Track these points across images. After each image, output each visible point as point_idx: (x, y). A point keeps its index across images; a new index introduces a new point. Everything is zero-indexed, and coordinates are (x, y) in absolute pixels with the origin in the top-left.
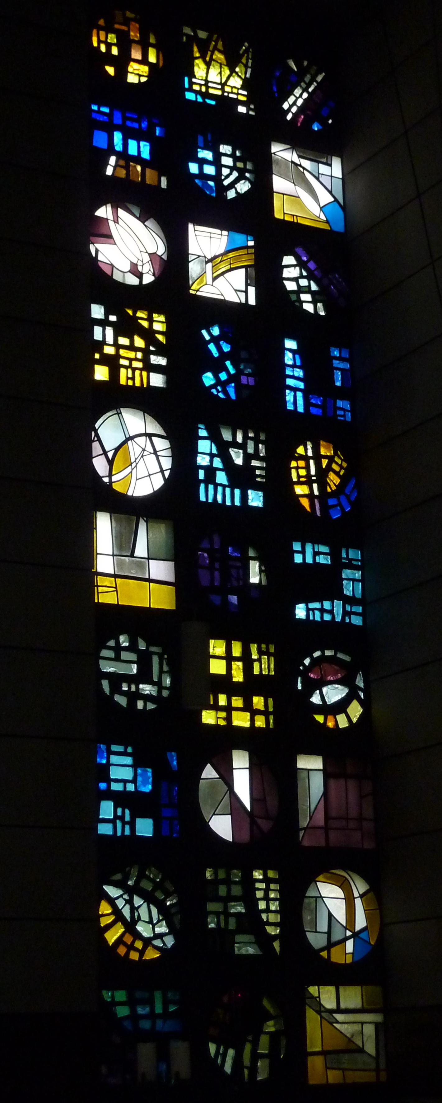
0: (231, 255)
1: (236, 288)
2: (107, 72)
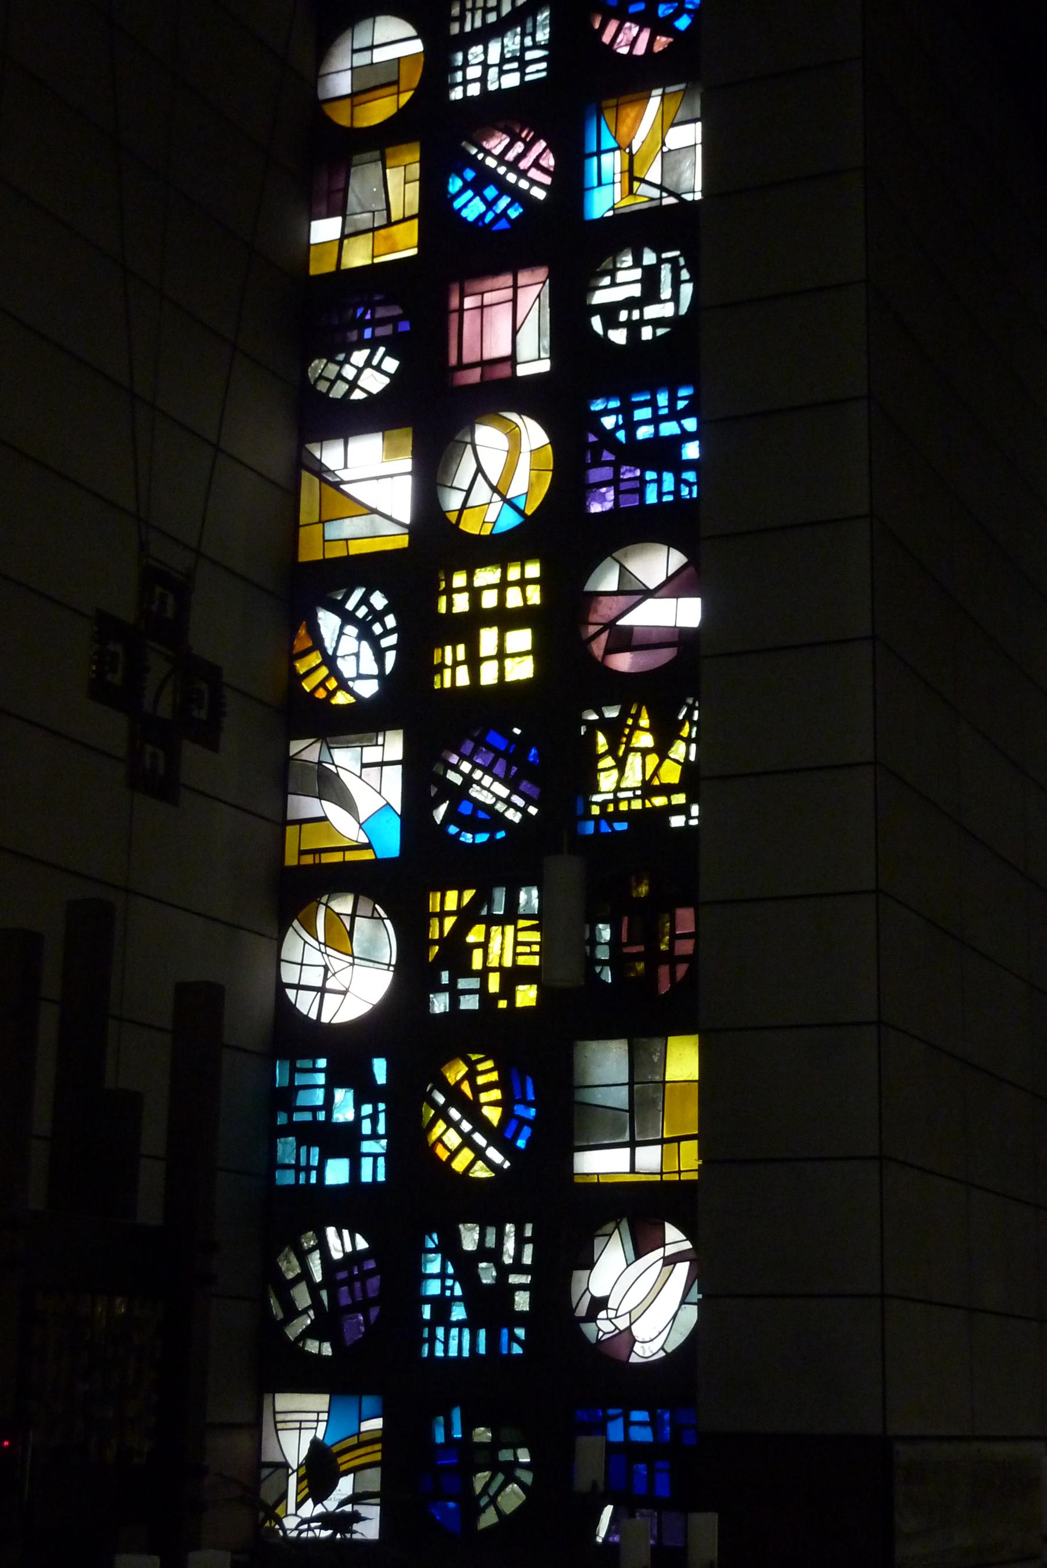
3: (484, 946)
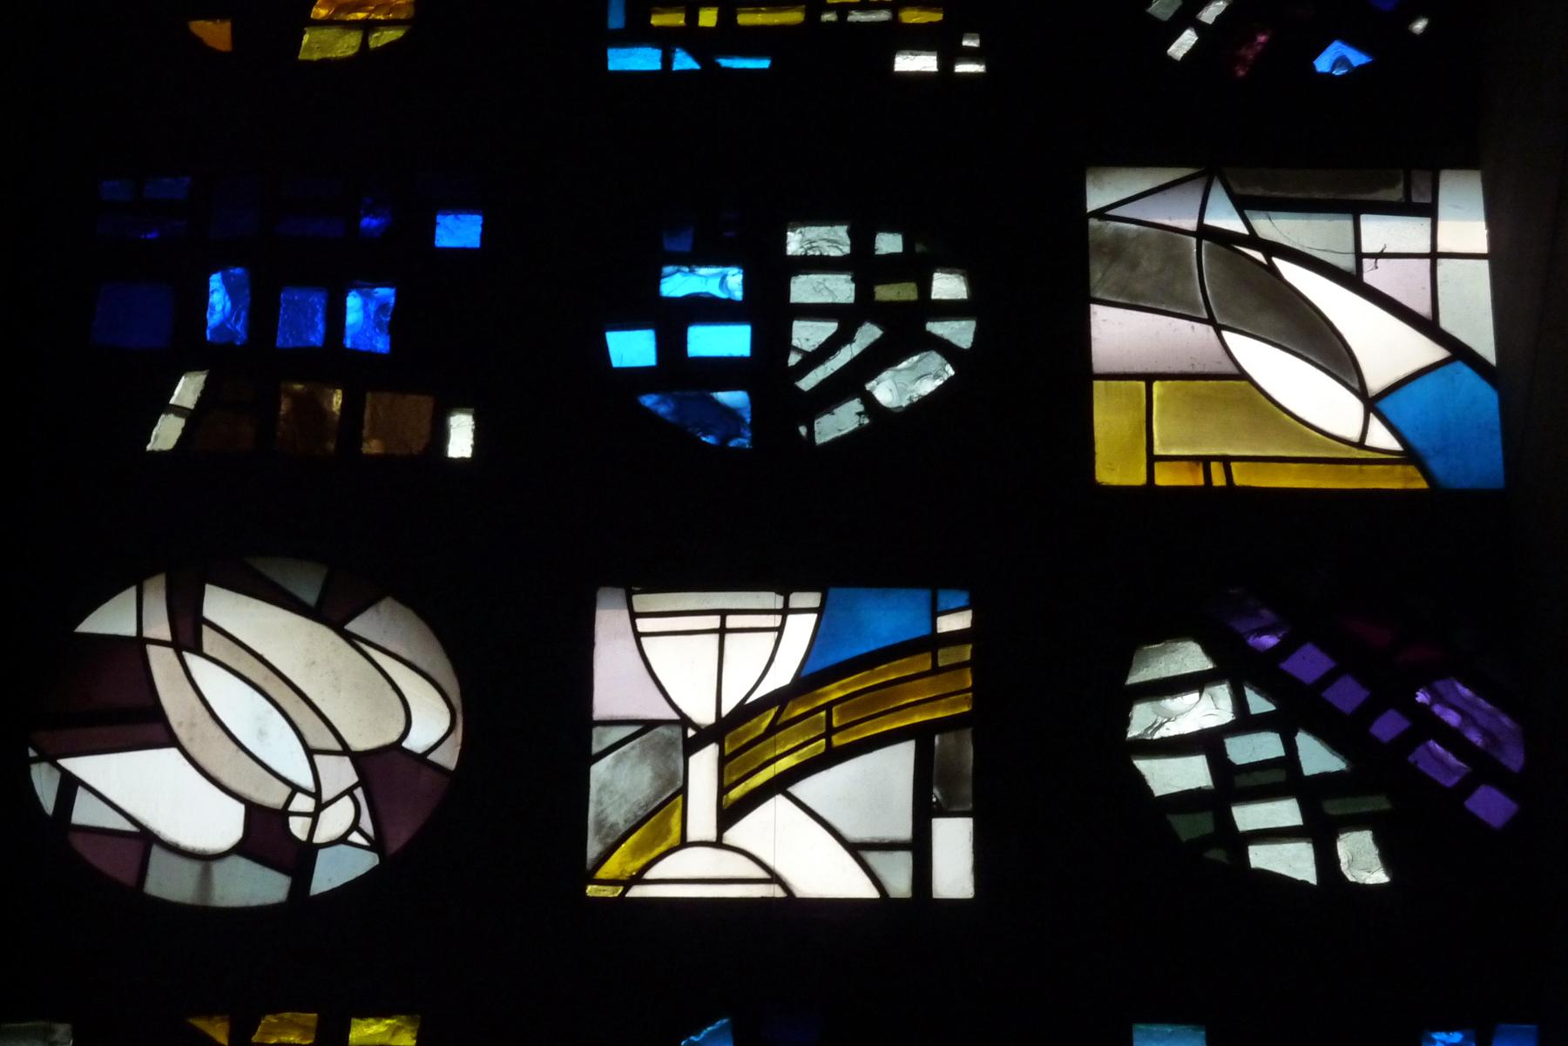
0: (834, 692)
1: (854, 833)
2: (197, 41)
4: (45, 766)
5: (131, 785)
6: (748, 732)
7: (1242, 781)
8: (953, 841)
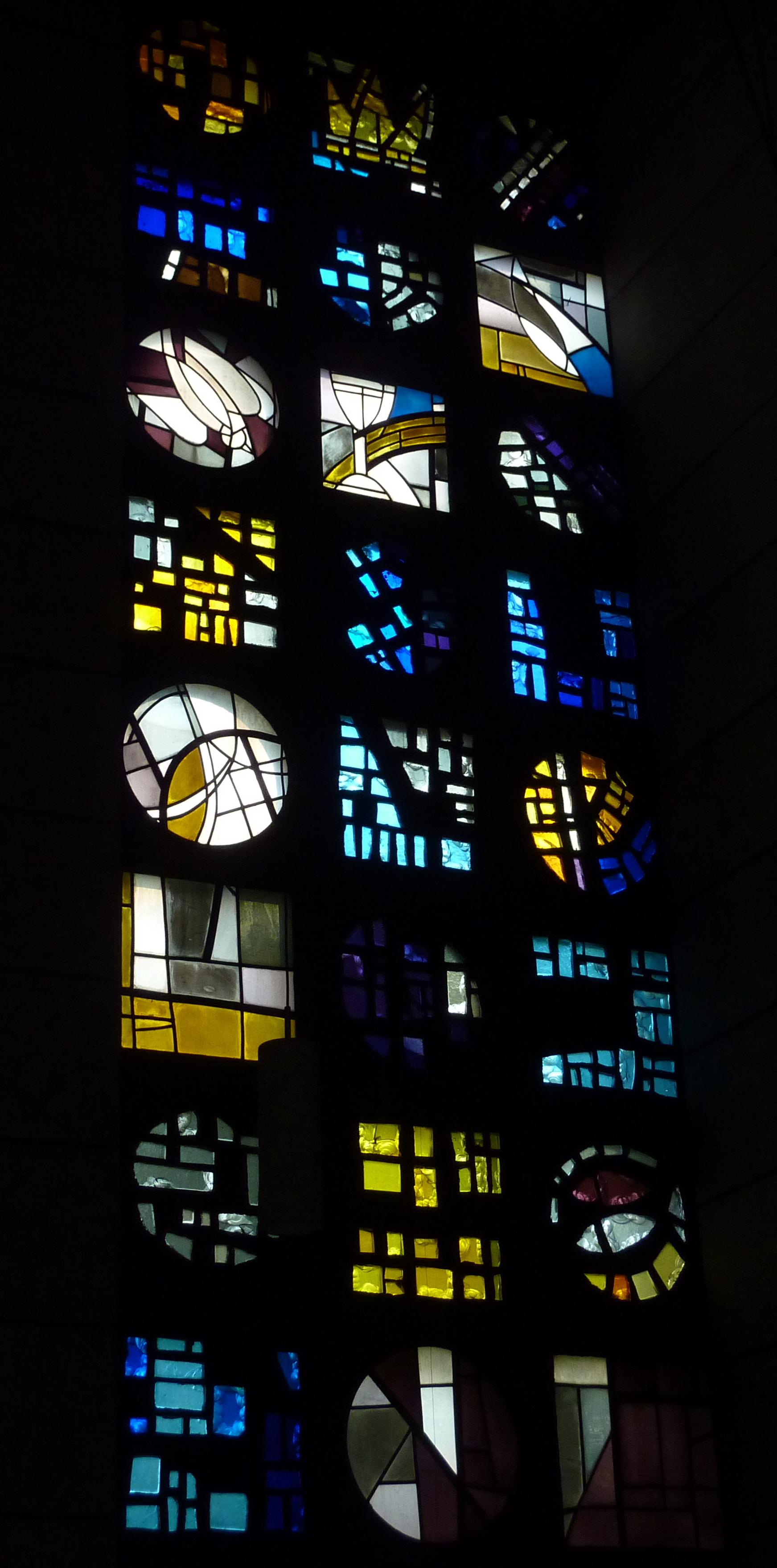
0: (401, 426)
1: (411, 482)
3: (208, 575)
4: (133, 396)
5: (160, 410)
6: (374, 435)
7: (537, 488)
8: (442, 488)
